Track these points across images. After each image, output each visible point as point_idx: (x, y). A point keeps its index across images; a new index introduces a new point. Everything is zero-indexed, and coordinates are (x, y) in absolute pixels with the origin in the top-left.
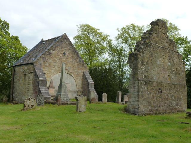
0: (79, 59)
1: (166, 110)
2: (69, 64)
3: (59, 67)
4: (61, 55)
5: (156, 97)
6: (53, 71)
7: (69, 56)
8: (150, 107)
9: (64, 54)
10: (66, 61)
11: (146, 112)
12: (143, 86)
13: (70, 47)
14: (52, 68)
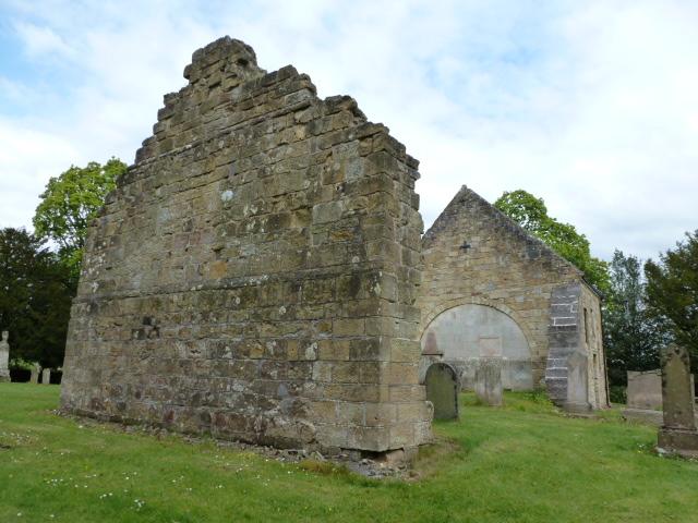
0: (524, 249)
1: (169, 417)
2: (483, 274)
3: (449, 290)
4: (455, 254)
5: (127, 356)
6: (431, 305)
7: (483, 249)
8: (96, 391)
9: (465, 247)
10: (471, 267)
11: (79, 405)
12: (82, 320)
13: (485, 221)
14: (428, 298)
